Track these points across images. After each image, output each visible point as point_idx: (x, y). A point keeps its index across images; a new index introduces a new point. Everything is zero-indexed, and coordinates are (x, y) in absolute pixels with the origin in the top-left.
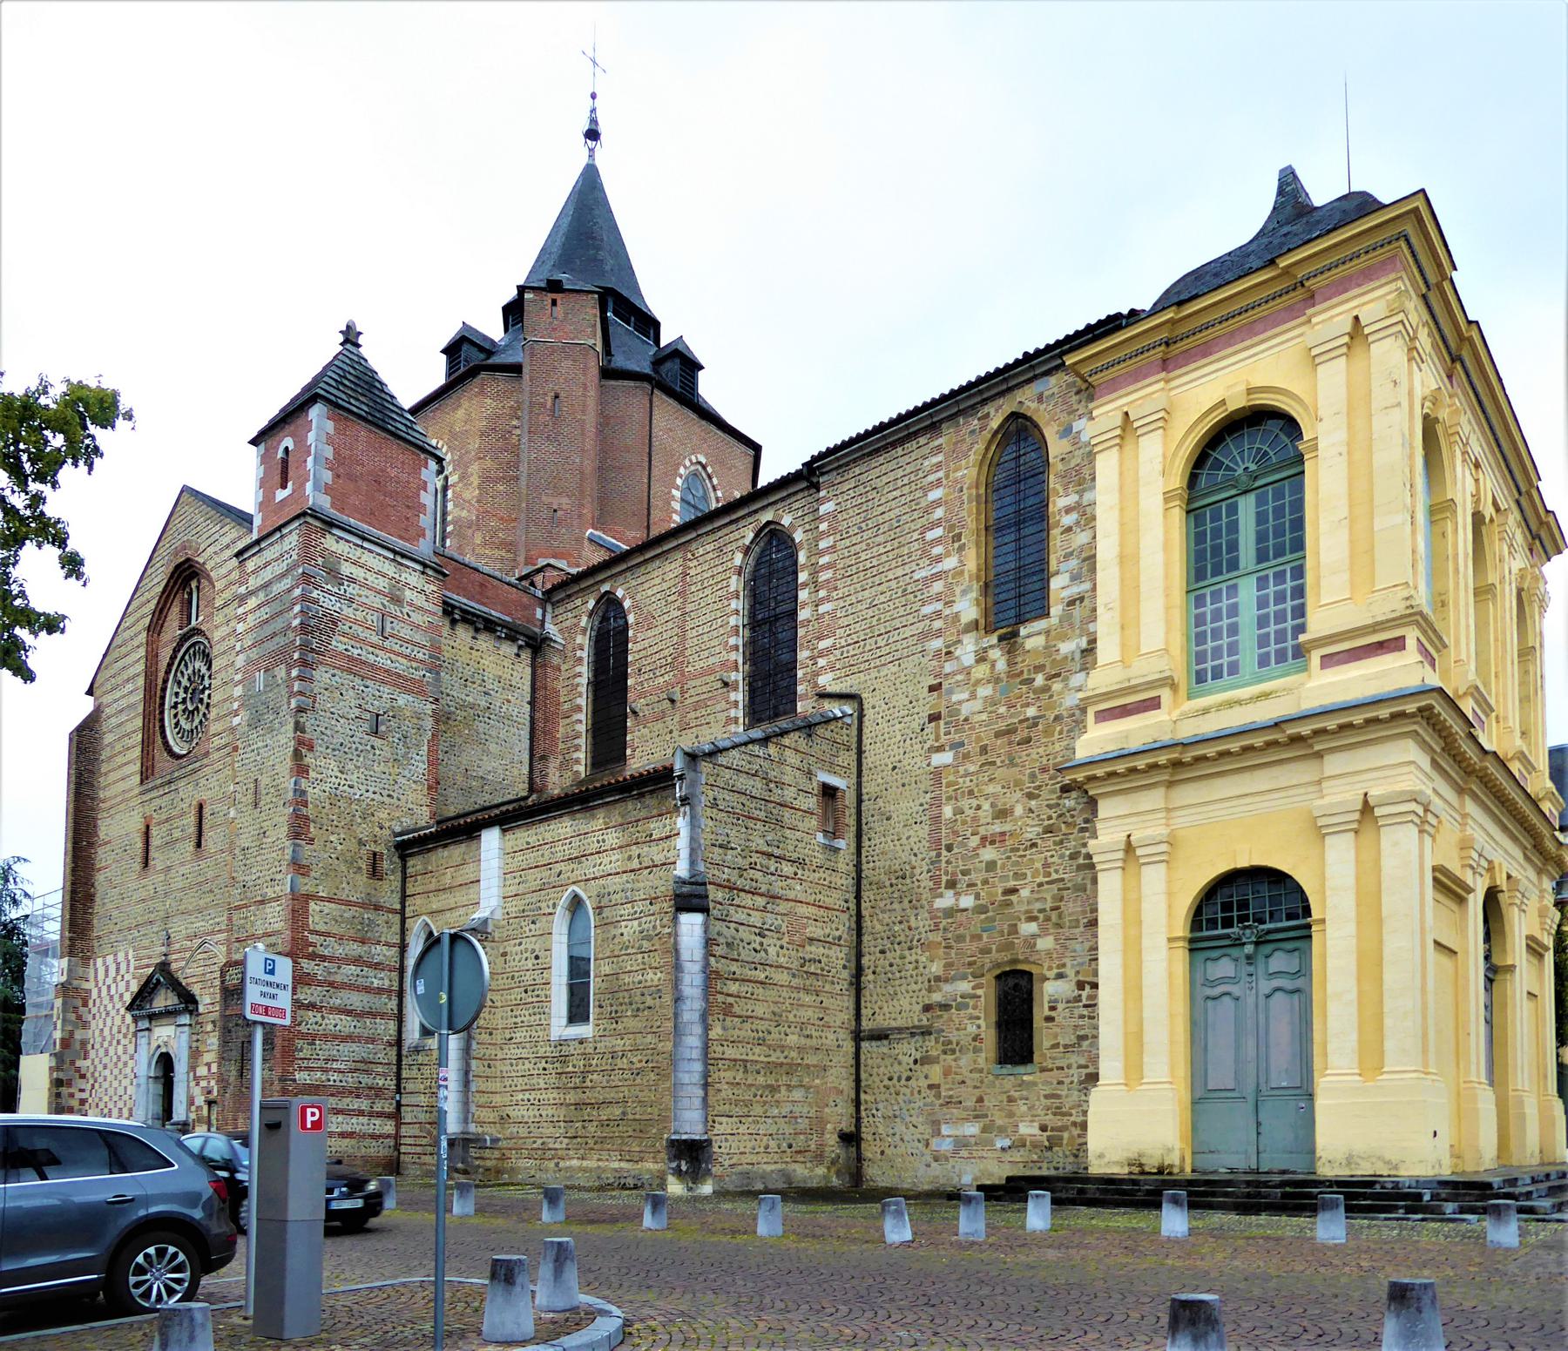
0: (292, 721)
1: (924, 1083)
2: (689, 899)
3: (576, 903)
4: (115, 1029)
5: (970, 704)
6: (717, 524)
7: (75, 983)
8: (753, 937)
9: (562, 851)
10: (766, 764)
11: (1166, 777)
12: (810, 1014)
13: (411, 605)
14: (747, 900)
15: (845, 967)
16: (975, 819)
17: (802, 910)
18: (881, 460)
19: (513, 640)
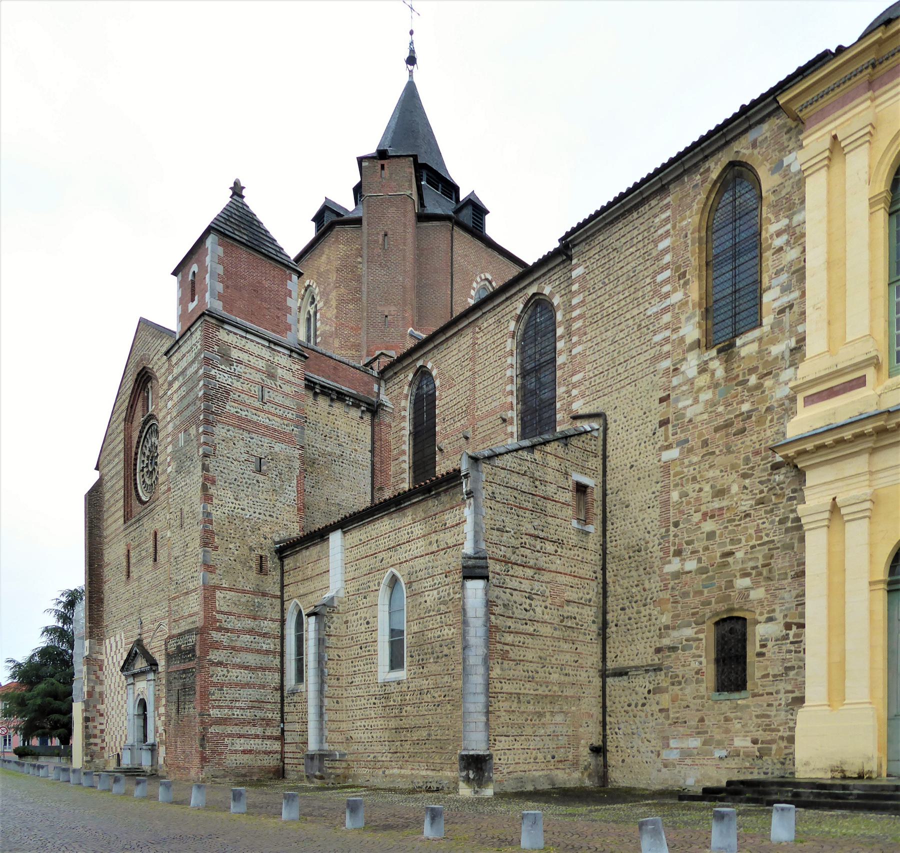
0: (200, 464)
1: (656, 708)
2: (474, 570)
3: (394, 580)
4: (117, 684)
5: (692, 408)
6: (496, 303)
7: (94, 656)
8: (524, 600)
9: (384, 543)
10: (533, 466)
11: (870, 445)
12: (568, 657)
13: (282, 379)
14: (519, 571)
15: (594, 622)
16: (698, 499)
17: (561, 579)
18: (620, 225)
19: (358, 407)
